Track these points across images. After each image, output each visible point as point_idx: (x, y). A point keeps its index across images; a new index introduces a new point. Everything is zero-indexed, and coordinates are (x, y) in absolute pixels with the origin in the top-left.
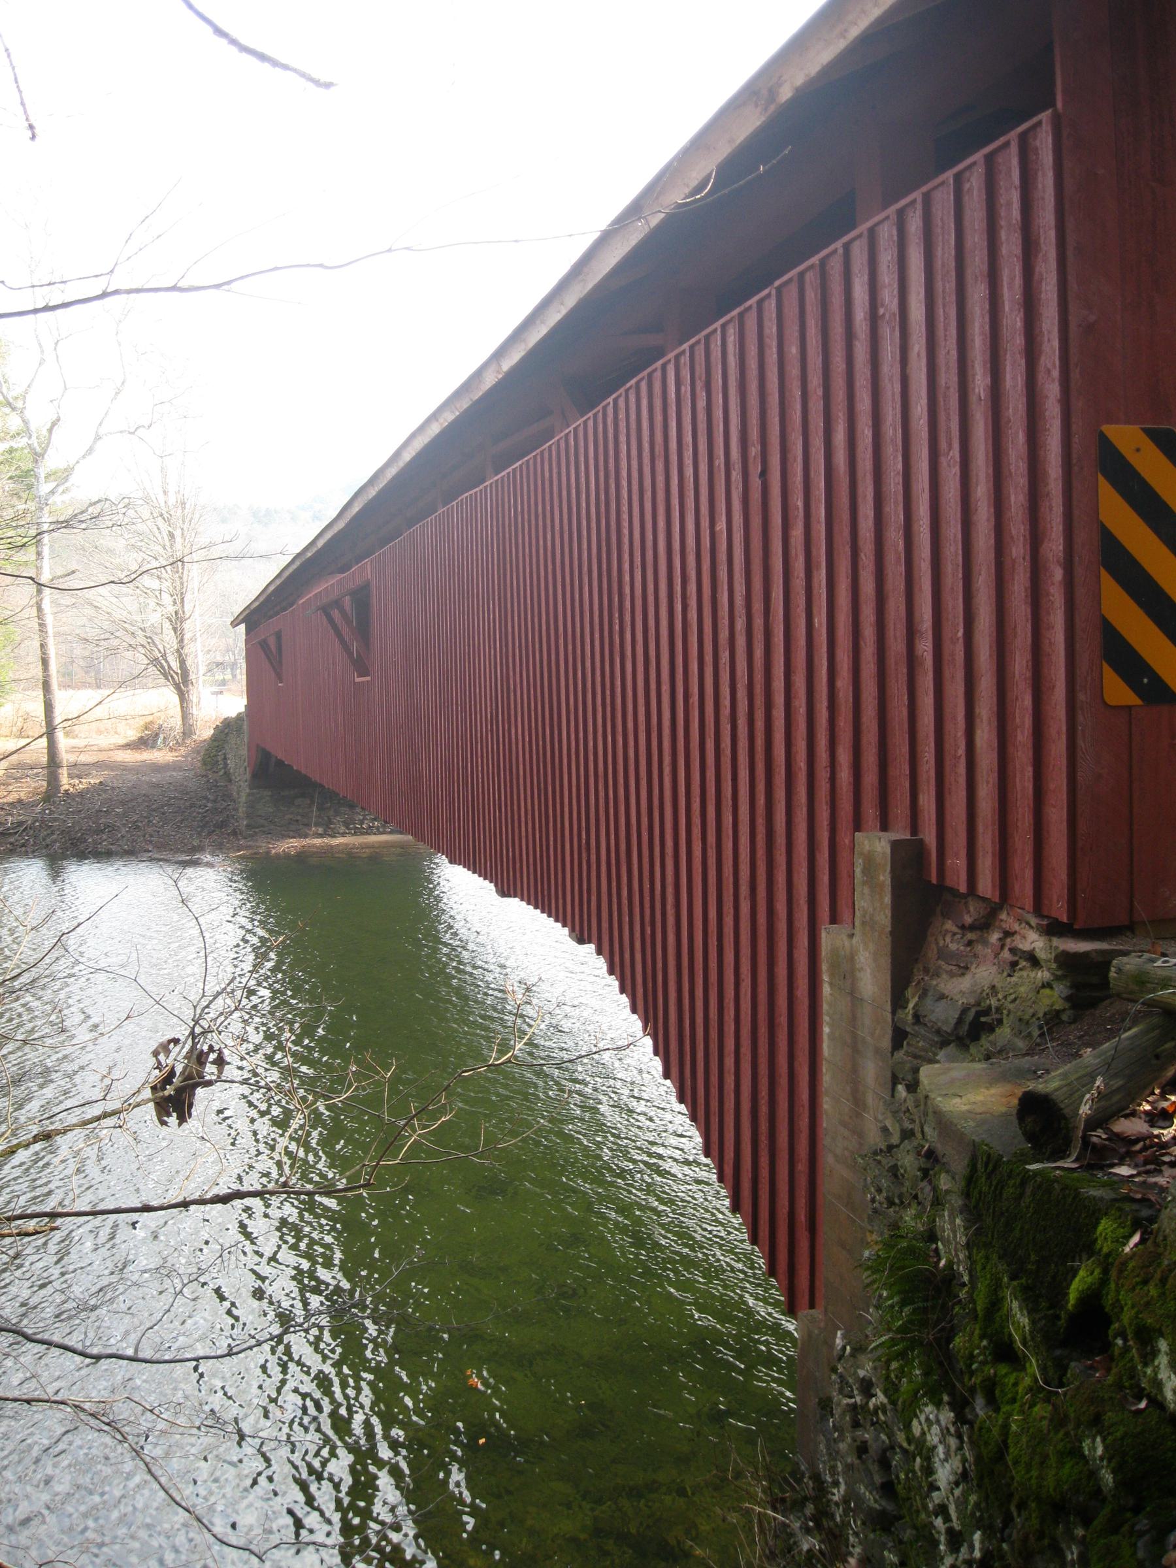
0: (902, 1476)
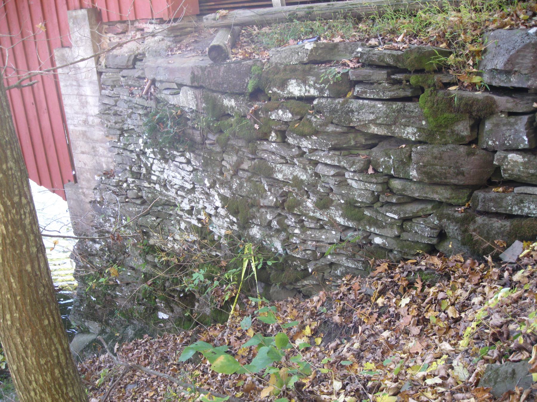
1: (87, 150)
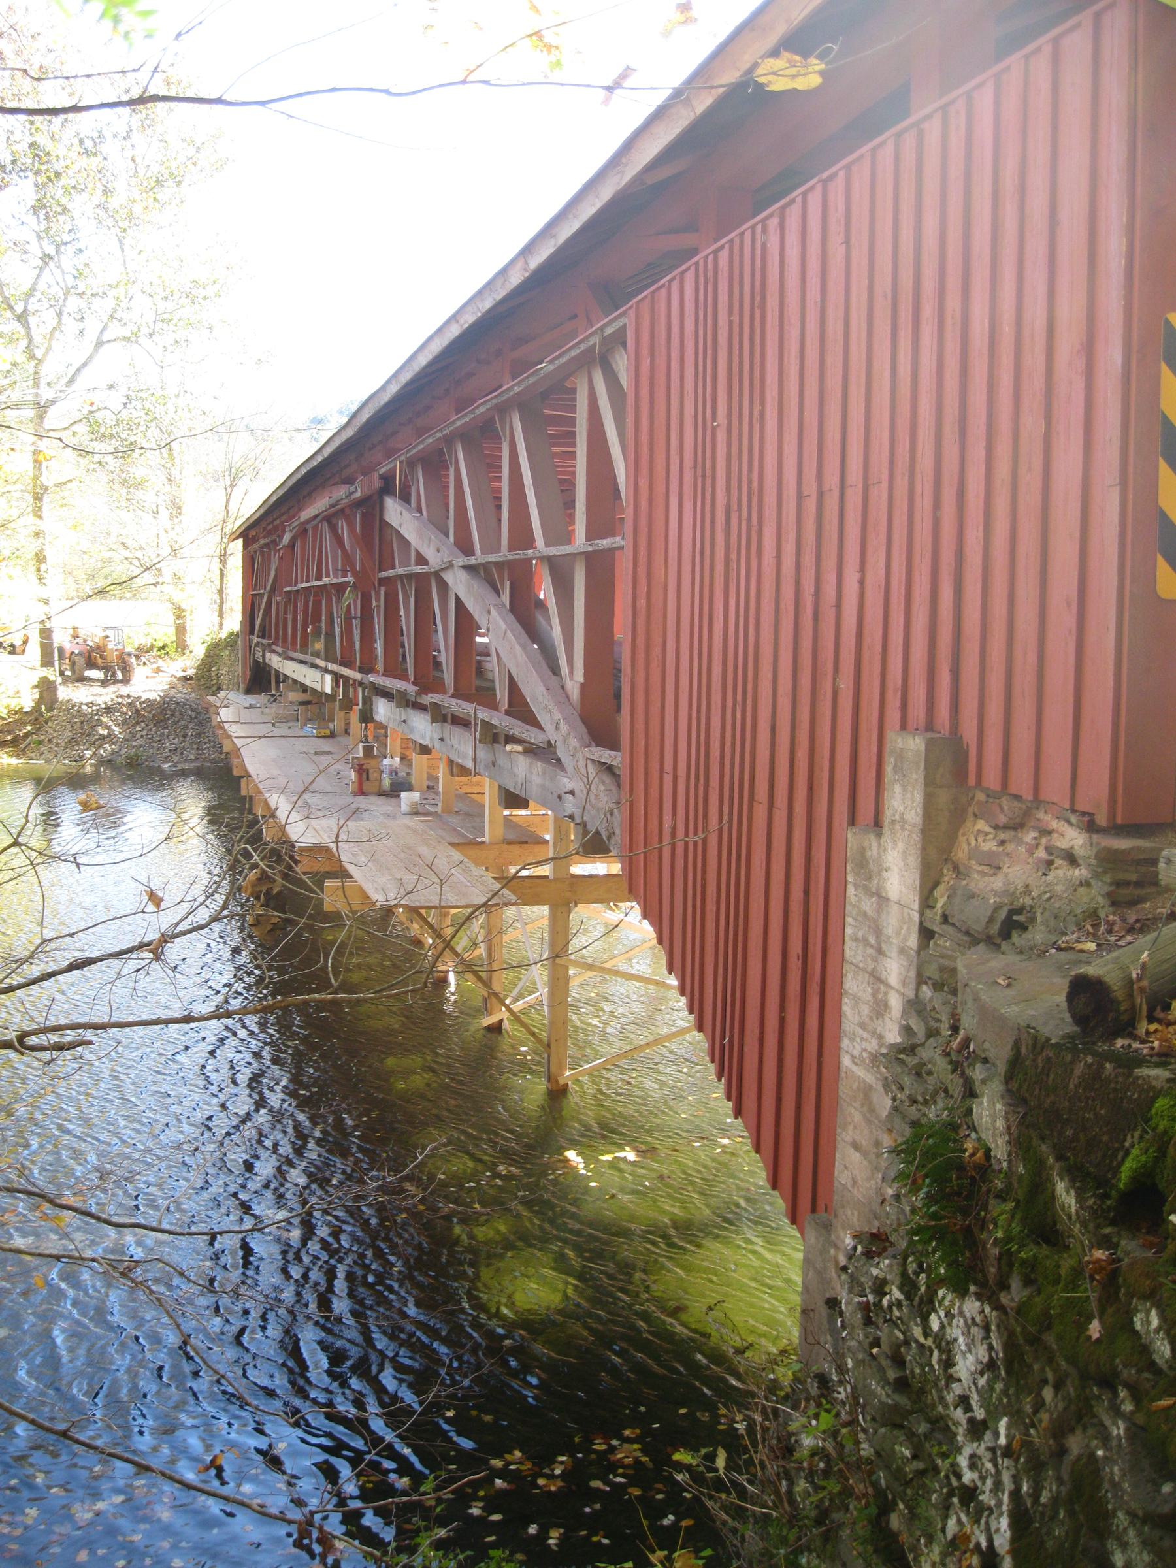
0: (917, 1371)
1: (864, 1143)
